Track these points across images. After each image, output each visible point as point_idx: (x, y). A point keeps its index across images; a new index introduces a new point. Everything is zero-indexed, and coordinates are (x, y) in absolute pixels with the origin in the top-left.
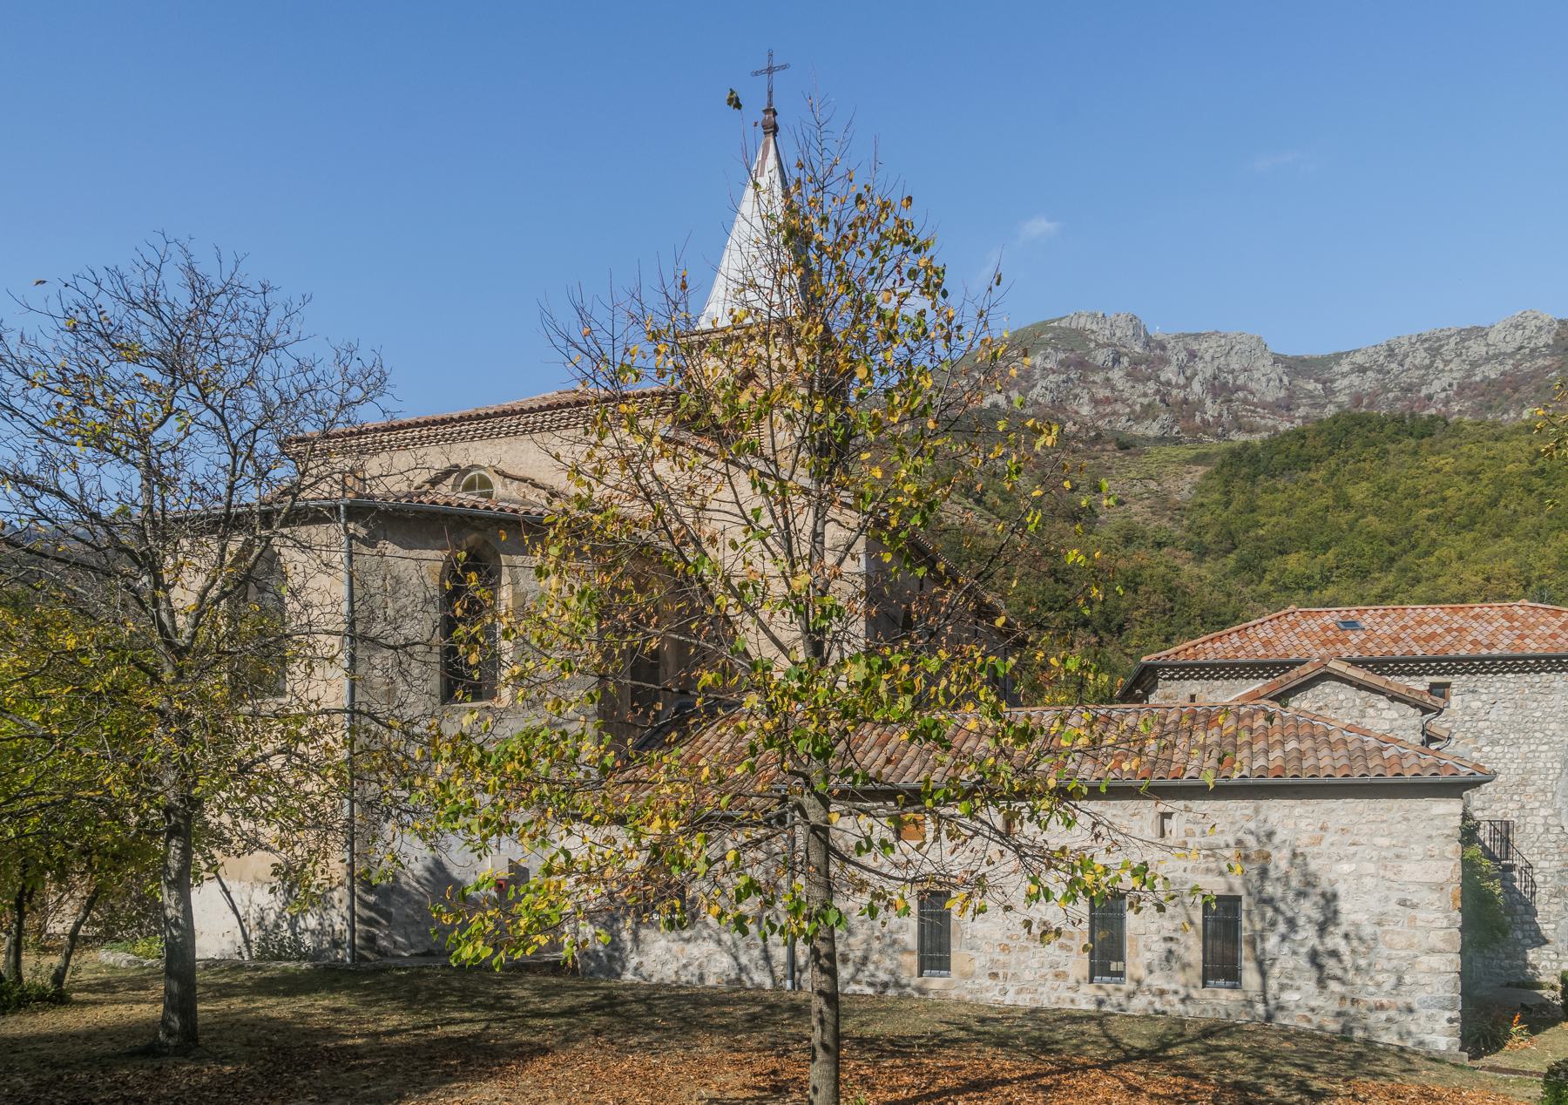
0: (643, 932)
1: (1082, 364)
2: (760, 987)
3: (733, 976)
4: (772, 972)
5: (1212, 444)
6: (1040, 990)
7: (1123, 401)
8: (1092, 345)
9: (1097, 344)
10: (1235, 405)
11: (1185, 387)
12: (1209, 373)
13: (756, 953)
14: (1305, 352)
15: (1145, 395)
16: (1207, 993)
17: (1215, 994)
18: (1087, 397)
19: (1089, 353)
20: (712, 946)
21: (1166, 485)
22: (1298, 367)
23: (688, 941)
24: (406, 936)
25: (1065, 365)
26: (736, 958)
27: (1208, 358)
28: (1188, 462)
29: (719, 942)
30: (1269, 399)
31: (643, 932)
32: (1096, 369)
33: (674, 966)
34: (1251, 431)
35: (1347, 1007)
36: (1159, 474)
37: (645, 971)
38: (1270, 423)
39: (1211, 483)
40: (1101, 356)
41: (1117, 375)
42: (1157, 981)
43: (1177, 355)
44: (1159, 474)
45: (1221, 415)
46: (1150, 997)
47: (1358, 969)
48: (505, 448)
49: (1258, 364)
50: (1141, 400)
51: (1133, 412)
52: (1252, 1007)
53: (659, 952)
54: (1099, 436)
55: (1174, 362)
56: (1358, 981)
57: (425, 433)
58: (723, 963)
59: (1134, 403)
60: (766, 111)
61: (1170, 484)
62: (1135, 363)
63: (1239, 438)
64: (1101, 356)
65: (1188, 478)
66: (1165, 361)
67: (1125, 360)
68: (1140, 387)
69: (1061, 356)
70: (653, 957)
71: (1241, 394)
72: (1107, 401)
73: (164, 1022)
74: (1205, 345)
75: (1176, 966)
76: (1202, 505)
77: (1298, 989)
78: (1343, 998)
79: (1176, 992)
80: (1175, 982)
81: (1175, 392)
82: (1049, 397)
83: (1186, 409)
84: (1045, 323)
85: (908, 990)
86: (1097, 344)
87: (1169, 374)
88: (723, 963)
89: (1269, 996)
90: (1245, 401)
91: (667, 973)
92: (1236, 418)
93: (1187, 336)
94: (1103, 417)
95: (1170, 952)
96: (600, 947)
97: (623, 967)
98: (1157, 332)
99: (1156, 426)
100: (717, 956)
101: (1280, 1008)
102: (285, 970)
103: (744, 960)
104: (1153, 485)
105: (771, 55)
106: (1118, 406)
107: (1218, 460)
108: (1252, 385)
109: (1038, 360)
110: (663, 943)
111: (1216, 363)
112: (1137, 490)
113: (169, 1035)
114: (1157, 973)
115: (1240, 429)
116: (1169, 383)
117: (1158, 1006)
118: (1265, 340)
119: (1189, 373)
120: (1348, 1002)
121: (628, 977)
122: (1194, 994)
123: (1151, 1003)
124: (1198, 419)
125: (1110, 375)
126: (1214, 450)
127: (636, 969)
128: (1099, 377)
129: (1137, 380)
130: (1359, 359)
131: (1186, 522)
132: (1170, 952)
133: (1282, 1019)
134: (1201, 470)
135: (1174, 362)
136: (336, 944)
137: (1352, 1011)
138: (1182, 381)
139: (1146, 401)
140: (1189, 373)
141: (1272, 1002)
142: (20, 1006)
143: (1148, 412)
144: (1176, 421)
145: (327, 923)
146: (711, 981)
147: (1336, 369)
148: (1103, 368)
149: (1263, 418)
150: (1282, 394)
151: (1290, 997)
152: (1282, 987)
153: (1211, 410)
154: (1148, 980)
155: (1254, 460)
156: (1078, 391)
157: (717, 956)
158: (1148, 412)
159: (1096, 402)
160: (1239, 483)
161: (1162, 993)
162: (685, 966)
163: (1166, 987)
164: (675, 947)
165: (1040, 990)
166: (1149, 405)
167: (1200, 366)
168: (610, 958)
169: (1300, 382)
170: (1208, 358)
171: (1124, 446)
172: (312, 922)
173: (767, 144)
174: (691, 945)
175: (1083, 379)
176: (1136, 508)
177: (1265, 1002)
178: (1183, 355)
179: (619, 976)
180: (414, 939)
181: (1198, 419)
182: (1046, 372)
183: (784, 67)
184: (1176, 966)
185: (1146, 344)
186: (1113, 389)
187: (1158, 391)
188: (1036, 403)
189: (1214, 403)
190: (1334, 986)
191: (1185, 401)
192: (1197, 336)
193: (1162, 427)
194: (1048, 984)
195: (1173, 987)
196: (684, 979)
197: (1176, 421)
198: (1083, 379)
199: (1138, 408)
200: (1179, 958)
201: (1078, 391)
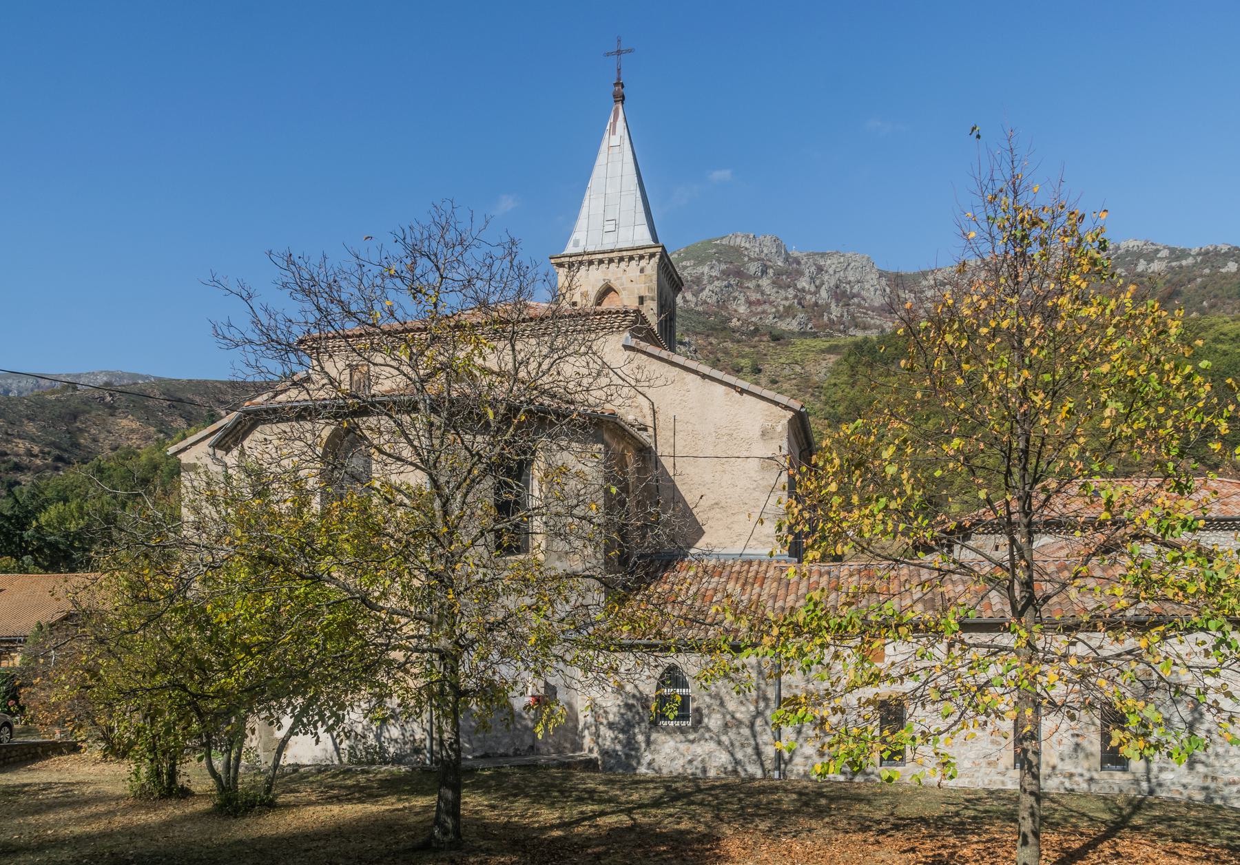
0: (654, 736)
1: (739, 274)
2: (752, 778)
3: (730, 768)
4: (762, 765)
5: (842, 340)
6: (976, 774)
7: (771, 303)
9: (750, 259)
10: (852, 308)
11: (815, 293)
13: (750, 750)
14: (903, 270)
15: (786, 299)
16: (1105, 775)
17: (1111, 775)
18: (743, 299)
19: (744, 265)
20: (712, 745)
21: (807, 369)
22: (898, 281)
23: (692, 742)
24: (470, 742)
26: (732, 755)
27: (831, 271)
28: (823, 351)
29: (719, 743)
30: (876, 304)
31: (654, 736)
32: (750, 278)
33: (681, 762)
34: (865, 328)
35: (1209, 782)
36: (802, 361)
37: (656, 766)
38: (878, 322)
39: (841, 368)
40: (753, 268)
42: (1068, 767)
43: (809, 270)
45: (842, 316)
46: (1061, 779)
47: (1217, 755)
49: (868, 277)
51: (778, 311)
52: (1139, 785)
53: (668, 751)
54: (757, 330)
55: (807, 274)
56: (1217, 764)
58: (723, 758)
60: (616, 85)
61: (810, 368)
62: (778, 274)
63: (860, 335)
64: (753, 268)
65: (824, 364)
66: (800, 273)
67: (771, 271)
68: (782, 292)
69: (723, 267)
70: (663, 755)
71: (856, 300)
72: (758, 302)
73: (437, 821)
75: (1081, 755)
76: (835, 385)
77: (1173, 770)
78: (1206, 776)
79: (1081, 775)
80: (1081, 767)
81: (808, 297)
82: (714, 298)
83: (818, 310)
84: (710, 241)
85: (872, 777)
86: (750, 259)
87: (803, 283)
88: (723, 758)
89: (1151, 776)
90: (859, 305)
91: (678, 766)
94: (756, 314)
95: (1077, 745)
96: (618, 747)
97: (639, 763)
98: (794, 252)
99: (795, 323)
100: (717, 753)
101: (1160, 785)
102: (391, 773)
103: (739, 756)
104: (798, 369)
106: (766, 307)
107: (846, 350)
108: (864, 293)
109: (706, 269)
110: (672, 743)
111: (837, 275)
112: (787, 372)
113: (445, 834)
114: (1067, 760)
116: (803, 290)
117: (1067, 785)
119: (818, 282)
120: (1209, 780)
122: (1096, 776)
123: (1063, 783)
124: (826, 318)
125: (760, 282)
126: (842, 342)
127: (649, 764)
128: (751, 284)
129: (780, 287)
130: (940, 277)
131: (823, 398)
132: (1077, 745)
133: (1163, 794)
134: (833, 358)
135: (807, 274)
136: (417, 751)
137: (1213, 785)
138: (813, 289)
139: (787, 303)
140: (818, 282)
141: (1154, 780)
142: (246, 811)
143: (788, 312)
144: (810, 319)
145: (408, 734)
146: (712, 773)
148: (754, 277)
151: (1167, 777)
152: (1161, 770)
153: (835, 311)
154: (1060, 766)
155: (873, 351)
156: (736, 294)
157: (717, 753)
158: (788, 312)
159: (750, 303)
160: (861, 369)
161: (1071, 775)
162: (690, 762)
163: (1073, 770)
164: (683, 747)
165: (976, 774)
167: (826, 278)
168: (628, 756)
170: (831, 271)
171: (777, 338)
172: (395, 732)
173: (617, 109)
174: (695, 745)
175: (740, 285)
177: (1149, 780)
178: (813, 269)
180: (475, 744)
181: (826, 318)
182: (712, 279)
183: (630, 51)
184: (1081, 755)
185: (786, 260)
186: (763, 293)
187: (796, 296)
188: (705, 302)
190: (1200, 768)
191: (816, 304)
192: (823, 255)
193: (800, 324)
194: (983, 770)
195: (1079, 770)
196: (689, 771)
197: (810, 319)
198: (740, 285)
199: (781, 308)
200: (1083, 749)
201: (736, 294)
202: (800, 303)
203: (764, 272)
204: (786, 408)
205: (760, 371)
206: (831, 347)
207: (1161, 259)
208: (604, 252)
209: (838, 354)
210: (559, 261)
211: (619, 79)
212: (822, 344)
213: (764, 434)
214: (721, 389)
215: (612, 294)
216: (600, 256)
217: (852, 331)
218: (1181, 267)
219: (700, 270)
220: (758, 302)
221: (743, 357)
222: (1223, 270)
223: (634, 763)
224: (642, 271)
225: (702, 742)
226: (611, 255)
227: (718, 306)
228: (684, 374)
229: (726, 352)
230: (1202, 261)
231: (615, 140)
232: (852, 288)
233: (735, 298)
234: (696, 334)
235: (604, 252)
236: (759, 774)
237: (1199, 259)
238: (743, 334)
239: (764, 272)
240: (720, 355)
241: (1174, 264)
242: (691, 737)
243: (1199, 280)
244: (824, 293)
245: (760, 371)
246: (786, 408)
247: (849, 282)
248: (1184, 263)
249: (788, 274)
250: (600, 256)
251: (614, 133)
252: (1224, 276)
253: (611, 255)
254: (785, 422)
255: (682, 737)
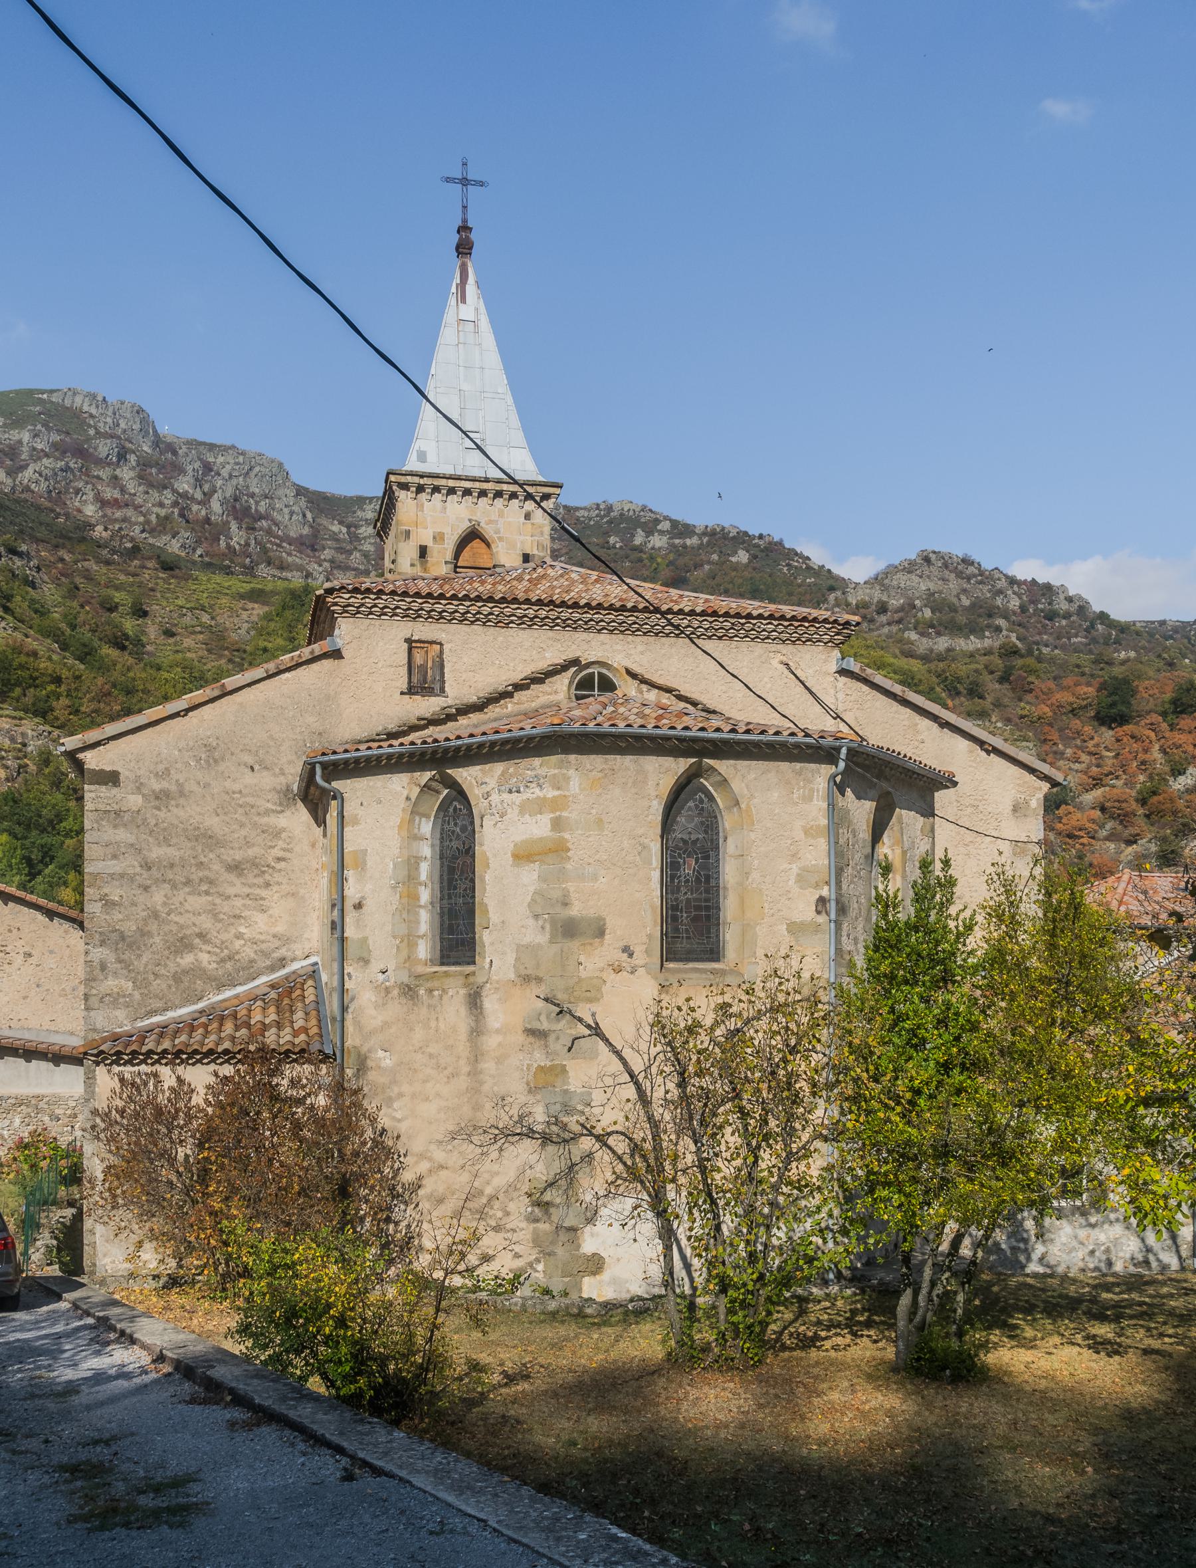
1: (81, 452)
3: (1140, 1257)
4: (1178, 1252)
7: (137, 507)
8: (92, 432)
9: (98, 432)
12: (229, 492)
15: (161, 505)
19: (89, 439)
23: (1093, 1226)
25: (59, 450)
26: (1143, 1240)
28: (242, 597)
32: (103, 462)
33: (1080, 1255)
39: (272, 625)
40: (104, 448)
41: (126, 474)
44: (211, 607)
45: (247, 544)
48: (640, 648)
49: (280, 492)
50: (156, 509)
51: (148, 522)
53: (1064, 1239)
55: (190, 472)
57: (543, 613)
59: (149, 512)
61: (224, 619)
62: (144, 464)
65: (245, 615)
67: (132, 458)
70: (1058, 1243)
71: (264, 523)
72: (116, 504)
74: (221, 459)
81: (195, 508)
82: (44, 485)
83: (208, 530)
87: (184, 484)
88: (1130, 1246)
92: (265, 551)
93: (204, 444)
97: (1029, 1259)
100: (1124, 1240)
105: (465, 164)
106: (129, 512)
111: (234, 482)
112: (188, 620)
115: (269, 564)
116: (184, 496)
118: (287, 467)
119: (206, 487)
121: (1034, 1267)
124: (223, 544)
128: (104, 473)
139: (163, 512)
140: (206, 487)
144: (198, 542)
147: (359, 513)
149: (289, 554)
150: (306, 531)
153: (237, 536)
159: (103, 503)
162: (1092, 1252)
164: (1082, 1233)
166: (167, 518)
169: (324, 521)
170: (225, 473)
174: (1097, 1230)
176: (188, 642)
178: (197, 465)
179: (1023, 1267)
182: (37, 455)
186: (123, 490)
187: (175, 504)
188: (27, 489)
189: (240, 528)
191: (207, 520)
192: (212, 447)
193: (183, 546)
197: (198, 542)
199: (153, 518)
201: (81, 485)
202: (182, 515)
203: (122, 456)
204: (1046, 778)
205: (145, 614)
206: (253, 591)
207: (661, 533)
208: (474, 480)
209: (264, 603)
210: (403, 479)
211: (465, 220)
212: (239, 584)
213: (1016, 809)
214: (963, 744)
215: (476, 543)
216: (468, 485)
217: (263, 570)
218: (685, 546)
219: (15, 435)
220: (116, 504)
221: (117, 588)
222: (734, 559)
223: (1022, 1258)
224: (528, 516)
225: (1106, 1226)
226: (485, 486)
227: (50, 499)
228: (917, 718)
229: (88, 576)
230: (709, 543)
231: (467, 312)
232: (257, 503)
233: (78, 491)
234: (39, 541)
235: (474, 480)
236: (1174, 1263)
237: (705, 540)
238: (114, 552)
239: (122, 456)
240: (78, 580)
241: (677, 541)
242: (1093, 1220)
243: (707, 567)
244: (216, 506)
245: (145, 614)
246: (1046, 778)
247: (252, 495)
248: (688, 542)
249: (161, 468)
250: (468, 485)
251: (464, 300)
252: (735, 567)
253: (485, 486)
254: (1041, 796)
255: (1082, 1221)
